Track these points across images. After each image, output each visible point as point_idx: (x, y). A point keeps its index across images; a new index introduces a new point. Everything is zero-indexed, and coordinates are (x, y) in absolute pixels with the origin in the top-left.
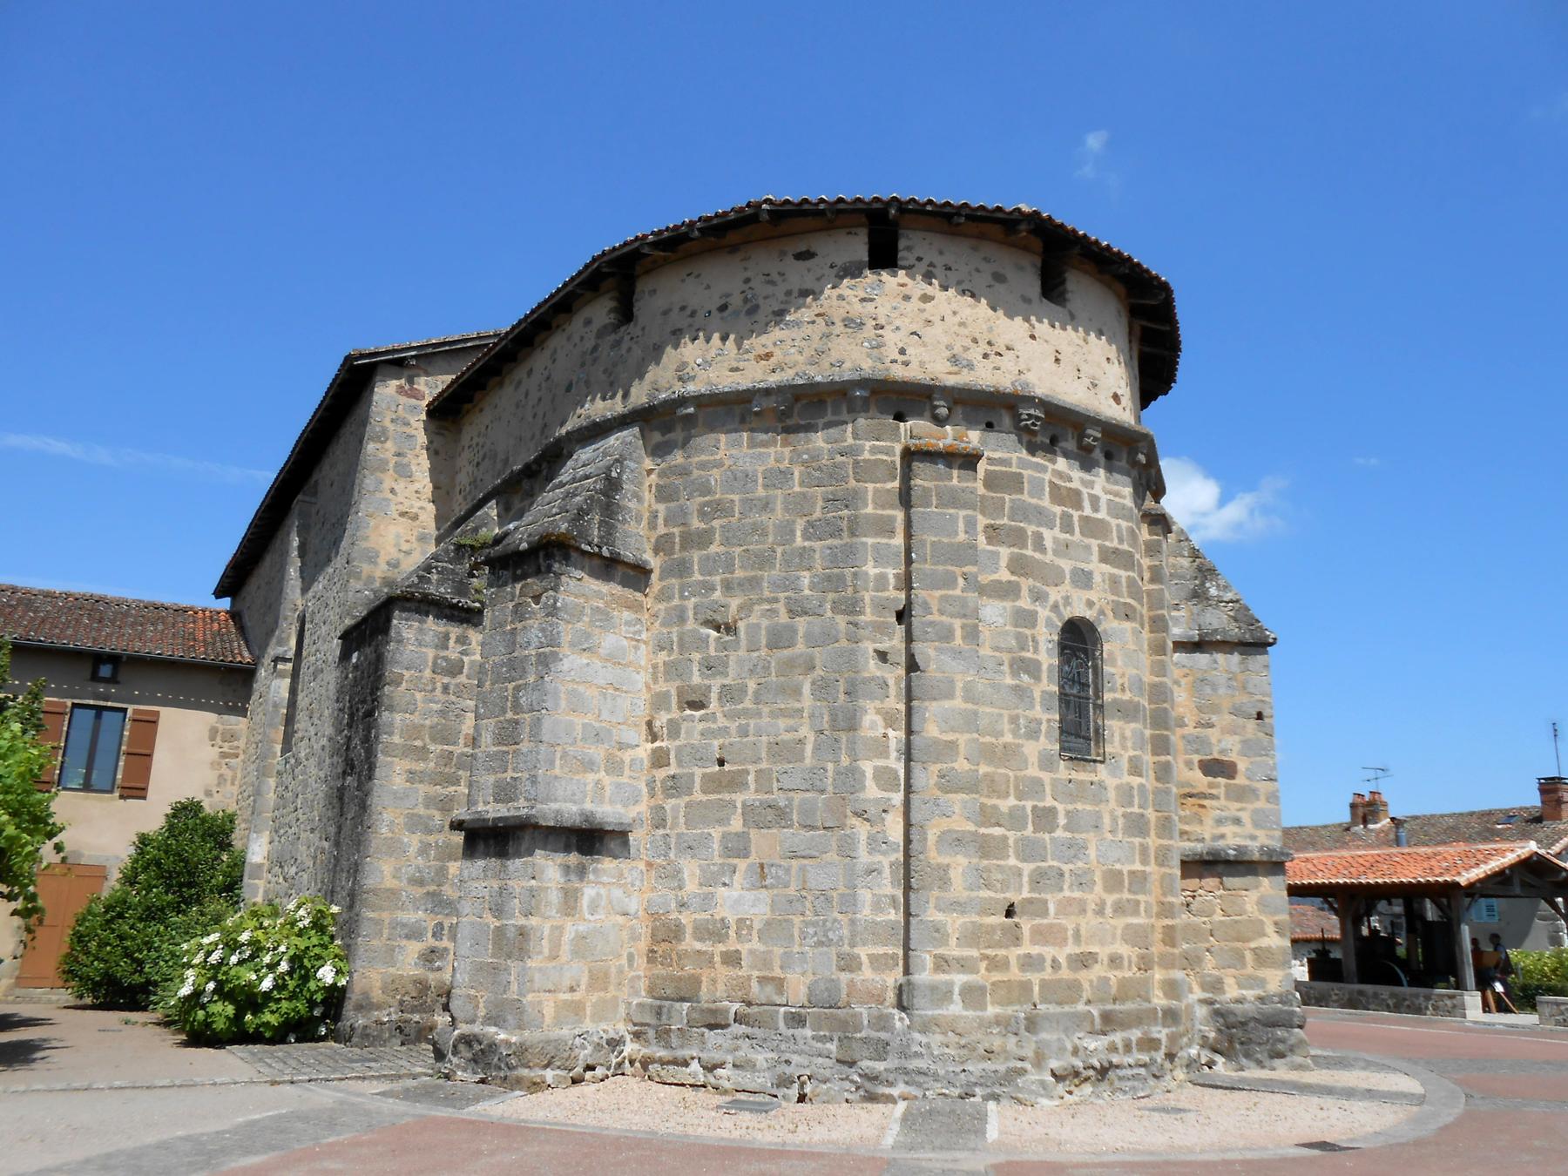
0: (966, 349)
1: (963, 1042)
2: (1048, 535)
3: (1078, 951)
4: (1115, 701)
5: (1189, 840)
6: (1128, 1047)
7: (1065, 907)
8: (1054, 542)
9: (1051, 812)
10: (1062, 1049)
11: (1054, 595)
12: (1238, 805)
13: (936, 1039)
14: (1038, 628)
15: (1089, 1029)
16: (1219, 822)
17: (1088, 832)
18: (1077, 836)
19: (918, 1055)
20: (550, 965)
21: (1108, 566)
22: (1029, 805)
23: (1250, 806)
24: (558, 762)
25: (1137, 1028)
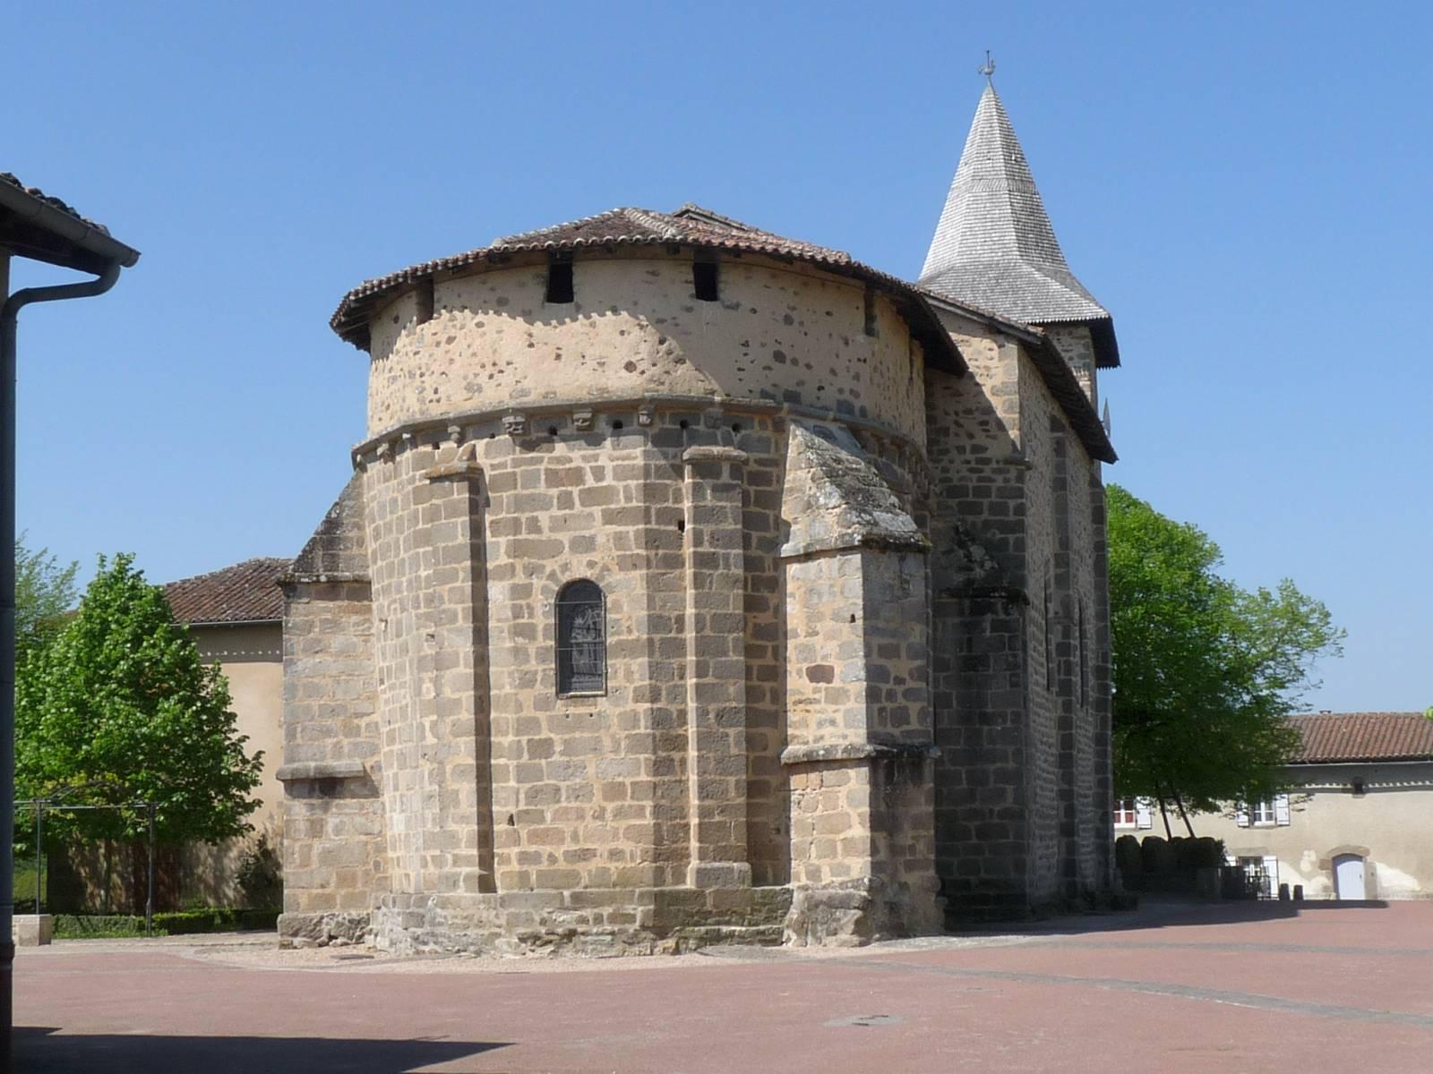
0: (476, 375)
1: (465, 914)
2: (544, 518)
3: (574, 847)
4: (619, 643)
5: (798, 743)
6: (598, 919)
7: (561, 815)
8: (551, 521)
9: (548, 743)
10: (530, 920)
11: (550, 565)
12: (834, 707)
13: (448, 912)
14: (533, 596)
15: (558, 906)
16: (820, 724)
17: (585, 754)
18: (574, 759)
19: (441, 924)
20: (301, 870)
21: (614, 526)
22: (524, 739)
23: (842, 707)
24: (298, 735)
25: (610, 906)
